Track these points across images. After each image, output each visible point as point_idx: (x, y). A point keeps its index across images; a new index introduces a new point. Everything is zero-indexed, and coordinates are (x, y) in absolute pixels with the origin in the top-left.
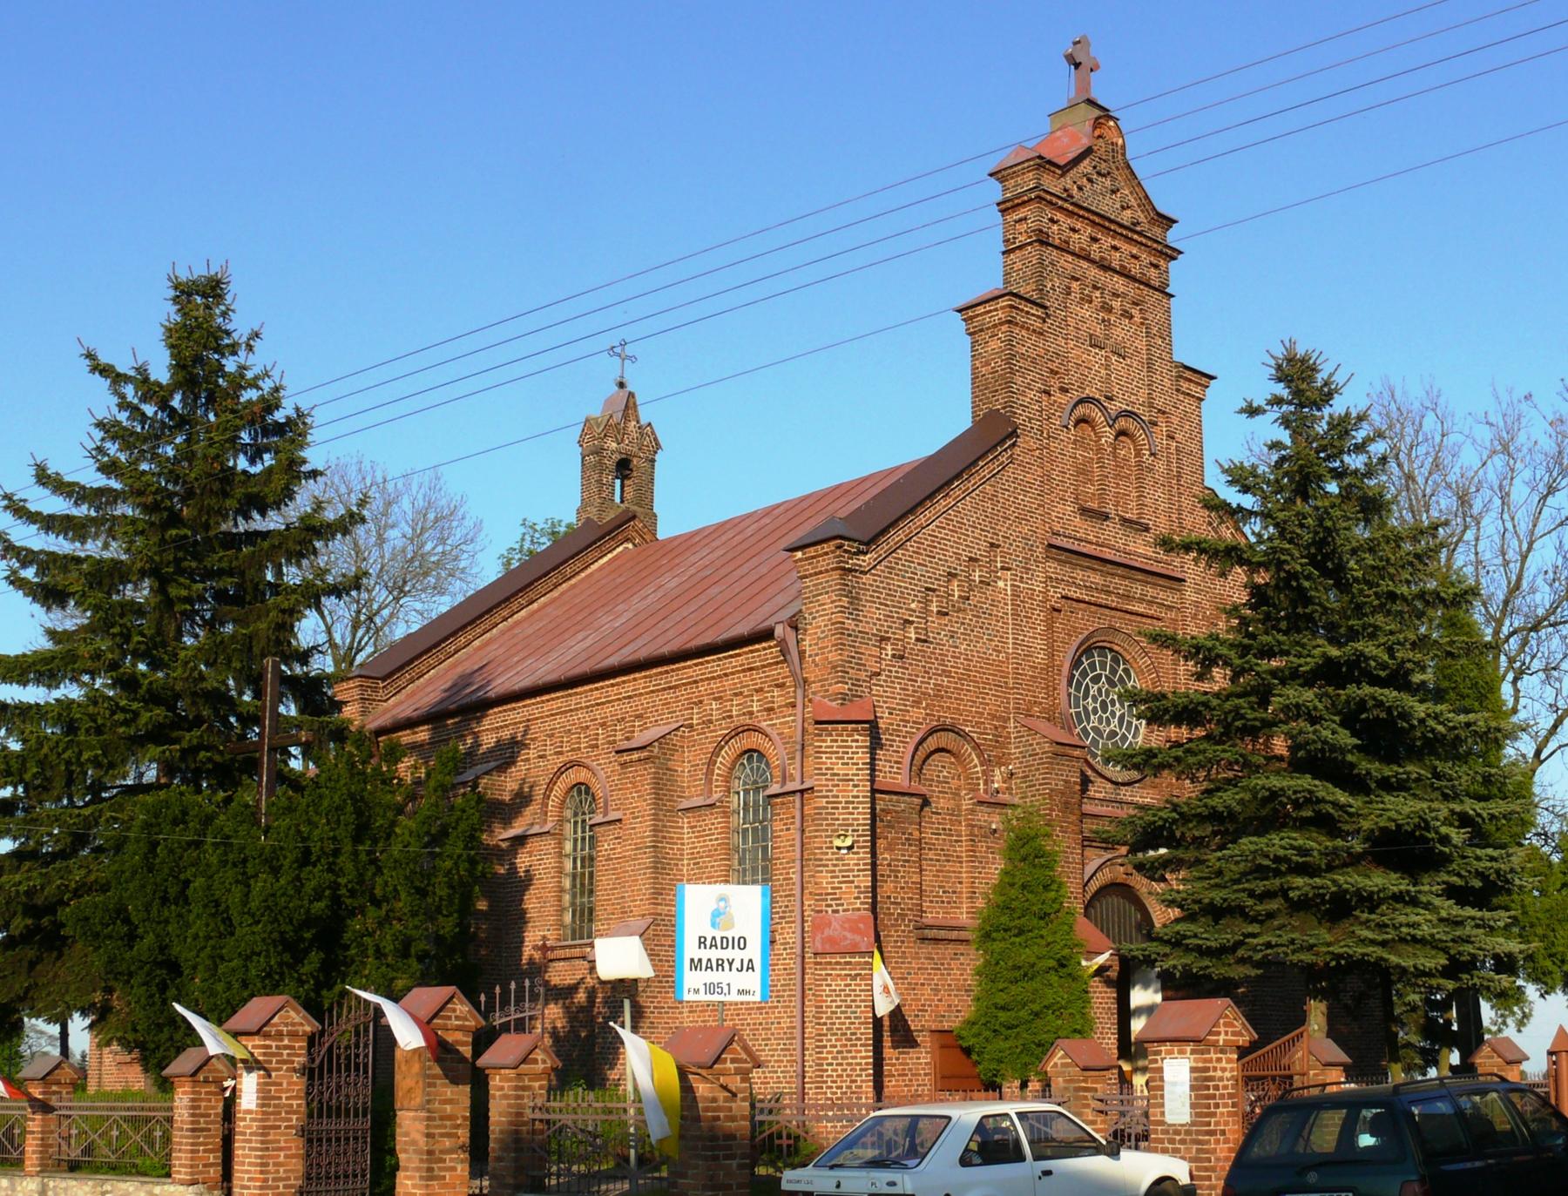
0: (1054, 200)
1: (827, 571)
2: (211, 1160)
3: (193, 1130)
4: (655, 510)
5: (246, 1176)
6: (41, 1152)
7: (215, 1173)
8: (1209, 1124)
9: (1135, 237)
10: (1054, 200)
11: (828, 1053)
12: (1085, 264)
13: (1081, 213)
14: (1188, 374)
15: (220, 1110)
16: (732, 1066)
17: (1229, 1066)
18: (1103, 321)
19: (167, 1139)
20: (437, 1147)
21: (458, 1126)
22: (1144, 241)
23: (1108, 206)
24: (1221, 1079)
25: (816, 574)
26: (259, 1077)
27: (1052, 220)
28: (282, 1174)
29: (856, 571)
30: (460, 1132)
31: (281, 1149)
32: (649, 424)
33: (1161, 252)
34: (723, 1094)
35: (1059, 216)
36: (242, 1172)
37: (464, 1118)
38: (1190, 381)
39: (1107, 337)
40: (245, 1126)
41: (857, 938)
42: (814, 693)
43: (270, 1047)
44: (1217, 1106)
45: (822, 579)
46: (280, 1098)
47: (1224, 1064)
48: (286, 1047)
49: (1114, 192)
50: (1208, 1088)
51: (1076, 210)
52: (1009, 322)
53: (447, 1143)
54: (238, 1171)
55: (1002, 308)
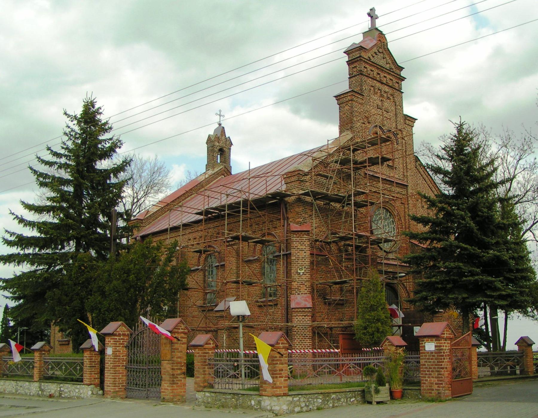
0: (366, 60)
1: (295, 181)
2: (96, 377)
3: (90, 367)
4: (231, 165)
5: (109, 382)
6: (39, 374)
7: (97, 381)
8: (442, 365)
9: (391, 73)
10: (366, 60)
11: (297, 341)
12: (375, 82)
13: (374, 65)
14: (408, 118)
15: (99, 360)
16: (282, 345)
17: (448, 345)
18: (381, 100)
19: (82, 370)
20: (175, 373)
21: (182, 366)
22: (394, 74)
23: (382, 63)
24: (445, 350)
25: (291, 182)
26: (113, 349)
27: (365, 67)
28: (121, 382)
29: (304, 181)
30: (183, 368)
31: (120, 373)
32: (229, 137)
33: (399, 78)
34: (278, 355)
35: (367, 66)
36: (107, 381)
37: (184, 363)
38: (409, 120)
39: (382, 106)
40: (108, 365)
41: (307, 303)
42: (291, 222)
43: (116, 339)
44: (444, 359)
45: (293, 184)
46: (120, 356)
47: (446, 345)
48: (122, 339)
49: (384, 58)
50: (441, 353)
51: (372, 64)
52: (352, 100)
53: (179, 372)
54: (106, 381)
55: (350, 96)
